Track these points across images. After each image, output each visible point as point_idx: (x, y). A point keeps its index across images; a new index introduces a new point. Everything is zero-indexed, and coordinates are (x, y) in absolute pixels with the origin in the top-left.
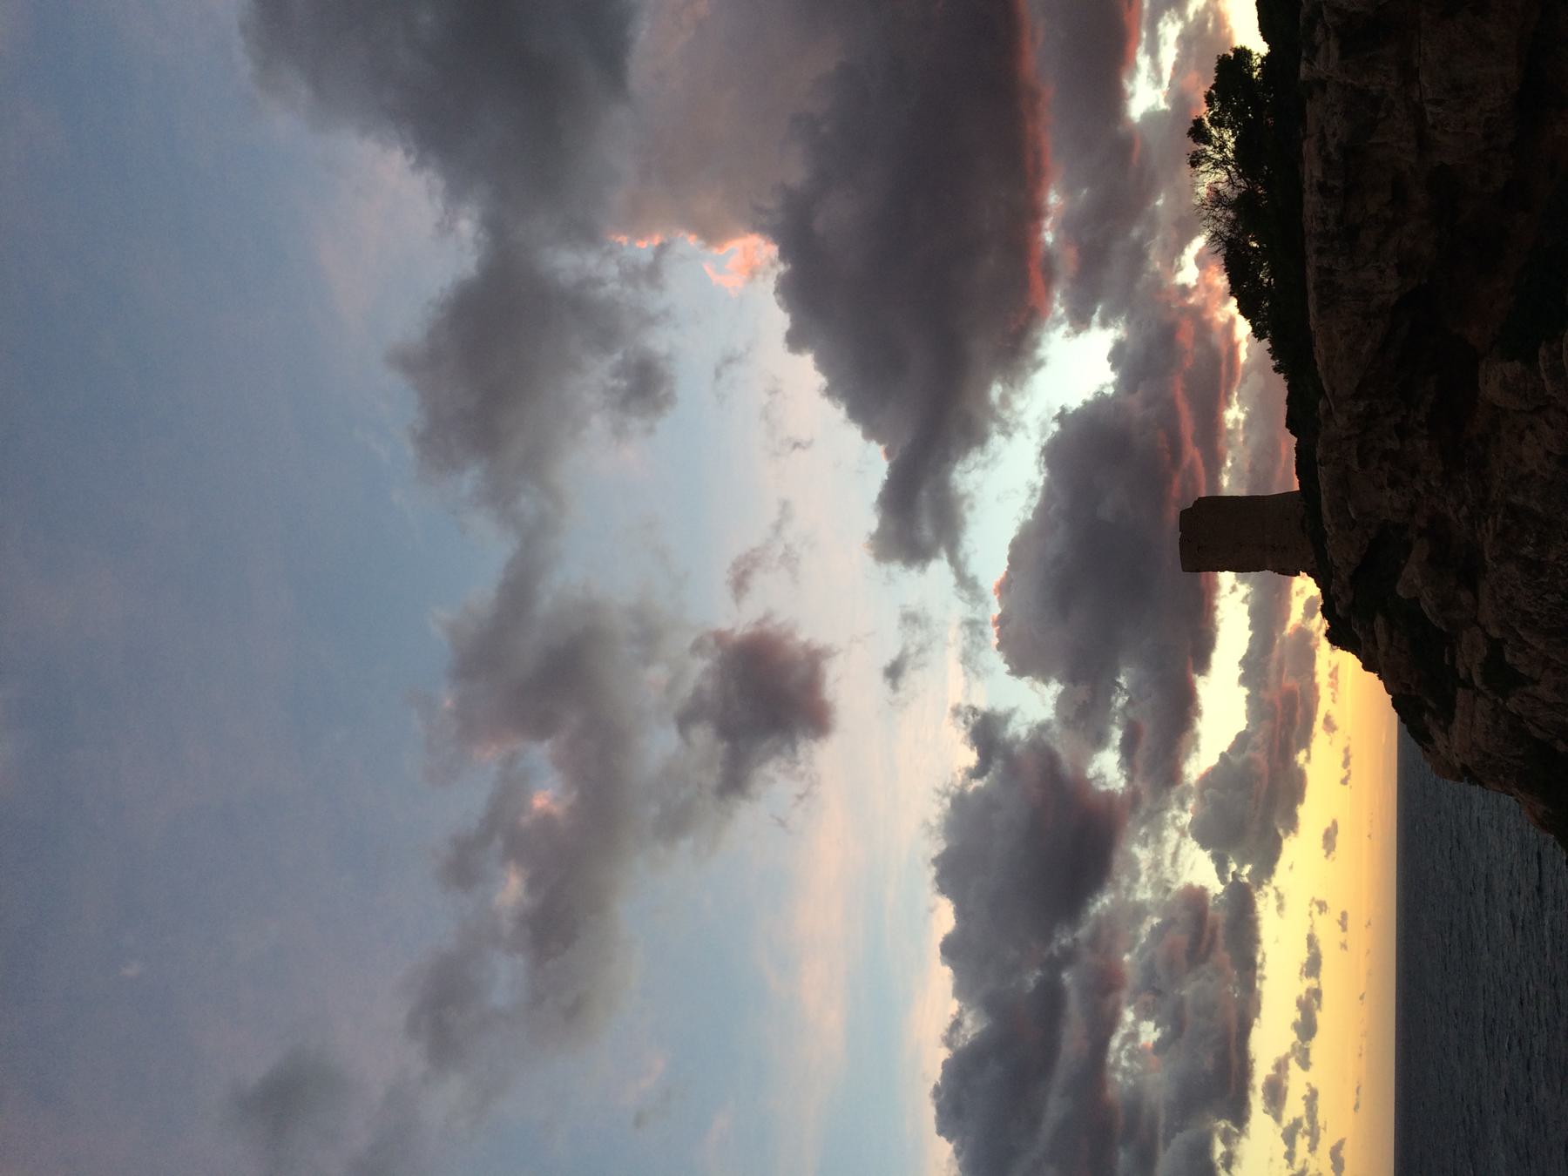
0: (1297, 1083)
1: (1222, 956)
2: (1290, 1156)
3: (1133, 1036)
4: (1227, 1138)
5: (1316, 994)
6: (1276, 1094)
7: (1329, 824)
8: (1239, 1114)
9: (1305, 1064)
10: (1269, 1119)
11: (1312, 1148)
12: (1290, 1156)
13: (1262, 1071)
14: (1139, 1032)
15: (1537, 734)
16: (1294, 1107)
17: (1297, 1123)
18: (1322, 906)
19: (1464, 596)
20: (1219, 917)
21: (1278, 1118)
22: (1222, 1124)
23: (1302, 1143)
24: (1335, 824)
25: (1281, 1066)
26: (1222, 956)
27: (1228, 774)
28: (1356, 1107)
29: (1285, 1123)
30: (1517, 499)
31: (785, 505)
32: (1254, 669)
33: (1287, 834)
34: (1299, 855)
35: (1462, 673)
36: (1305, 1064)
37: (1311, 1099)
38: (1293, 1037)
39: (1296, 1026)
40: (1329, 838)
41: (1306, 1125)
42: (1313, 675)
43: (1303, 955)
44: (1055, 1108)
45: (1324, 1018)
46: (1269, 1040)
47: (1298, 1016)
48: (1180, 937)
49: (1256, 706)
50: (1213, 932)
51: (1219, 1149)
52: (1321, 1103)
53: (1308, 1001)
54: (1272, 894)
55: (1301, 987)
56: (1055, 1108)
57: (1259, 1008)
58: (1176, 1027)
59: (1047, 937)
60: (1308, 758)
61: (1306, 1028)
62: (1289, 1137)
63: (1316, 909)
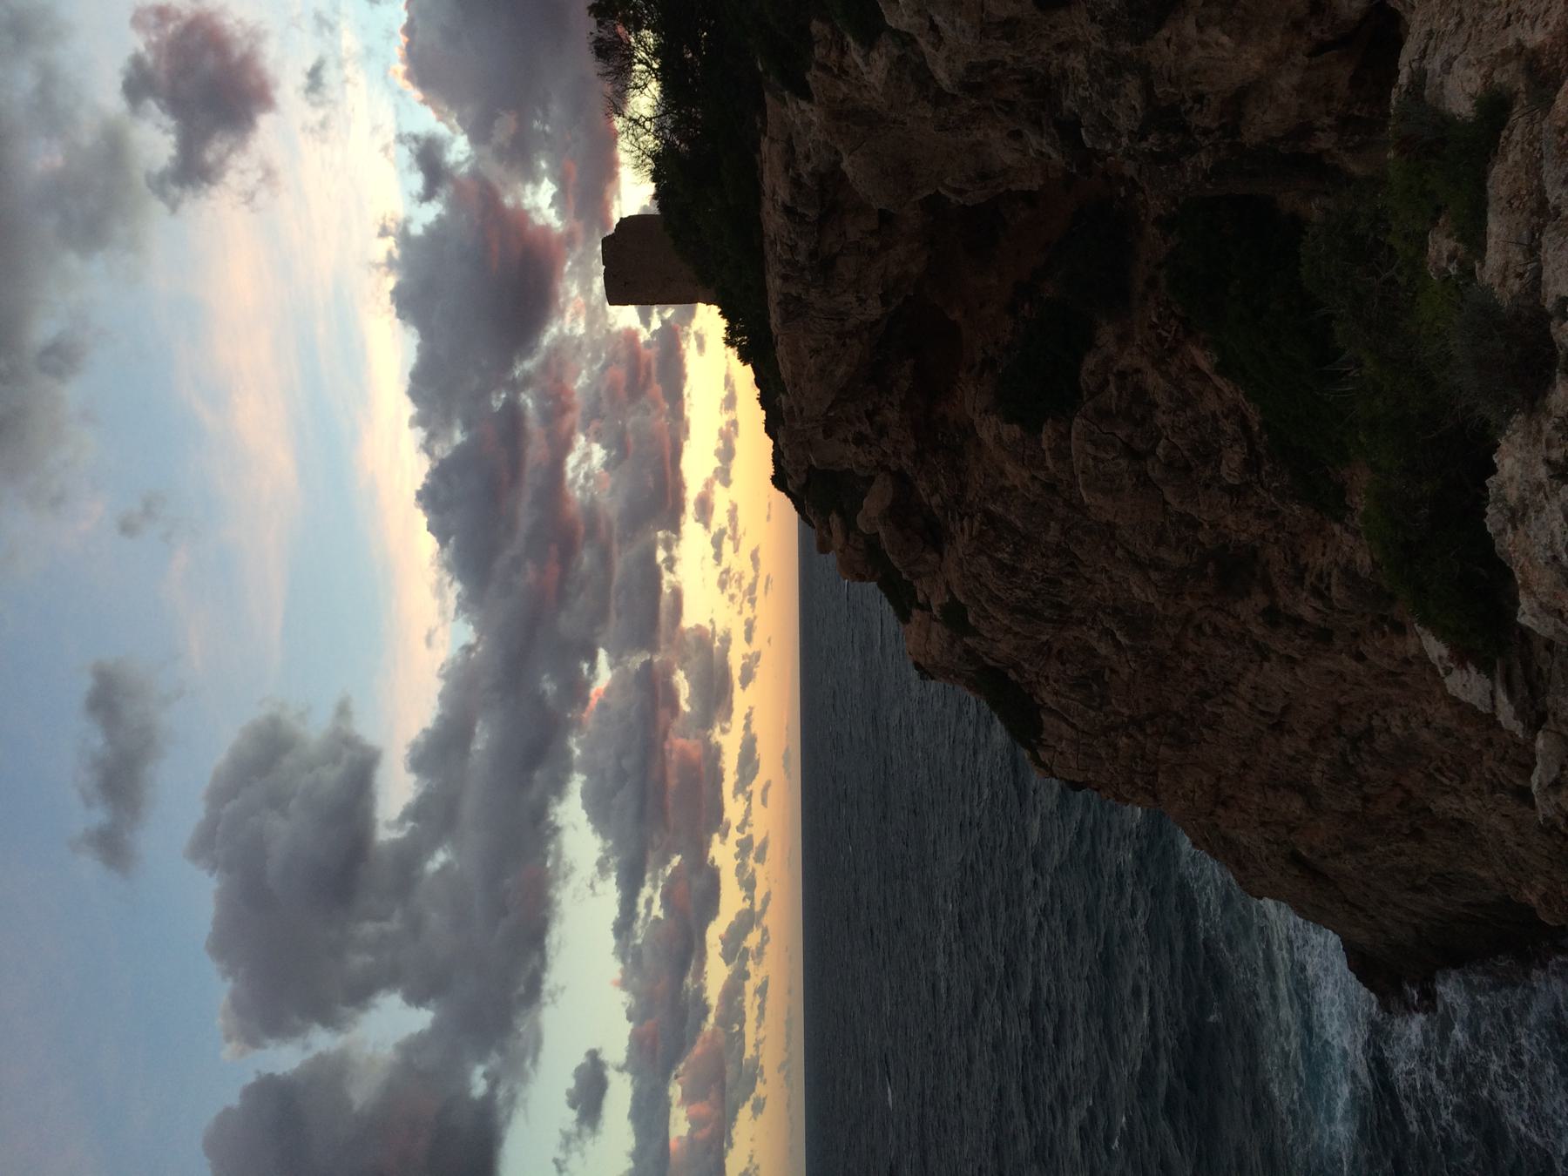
0: (721, 499)
1: (656, 388)
2: (718, 557)
3: (587, 456)
4: (668, 546)
5: (734, 424)
6: (705, 509)
8: (673, 524)
9: (727, 482)
10: (700, 526)
11: (736, 550)
12: (718, 557)
13: (692, 492)
14: (587, 460)
15: (990, 662)
16: (720, 518)
17: (722, 532)
19: (931, 557)
20: (652, 354)
21: (707, 526)
22: (660, 534)
23: (727, 546)
25: (708, 485)
26: (656, 388)
28: (768, 518)
29: (714, 528)
30: (997, 508)
31: (109, 698)
35: (921, 597)
36: (727, 482)
37: (733, 514)
38: (716, 463)
39: (718, 453)
41: (729, 531)
43: (724, 394)
44: (525, 515)
45: (739, 444)
46: (696, 464)
47: (721, 444)
48: (620, 373)
50: (648, 366)
51: (661, 555)
52: (741, 514)
54: (692, 337)
55: (721, 420)
56: (525, 515)
57: (687, 431)
58: (620, 449)
59: (508, 365)
61: (727, 454)
62: (717, 543)
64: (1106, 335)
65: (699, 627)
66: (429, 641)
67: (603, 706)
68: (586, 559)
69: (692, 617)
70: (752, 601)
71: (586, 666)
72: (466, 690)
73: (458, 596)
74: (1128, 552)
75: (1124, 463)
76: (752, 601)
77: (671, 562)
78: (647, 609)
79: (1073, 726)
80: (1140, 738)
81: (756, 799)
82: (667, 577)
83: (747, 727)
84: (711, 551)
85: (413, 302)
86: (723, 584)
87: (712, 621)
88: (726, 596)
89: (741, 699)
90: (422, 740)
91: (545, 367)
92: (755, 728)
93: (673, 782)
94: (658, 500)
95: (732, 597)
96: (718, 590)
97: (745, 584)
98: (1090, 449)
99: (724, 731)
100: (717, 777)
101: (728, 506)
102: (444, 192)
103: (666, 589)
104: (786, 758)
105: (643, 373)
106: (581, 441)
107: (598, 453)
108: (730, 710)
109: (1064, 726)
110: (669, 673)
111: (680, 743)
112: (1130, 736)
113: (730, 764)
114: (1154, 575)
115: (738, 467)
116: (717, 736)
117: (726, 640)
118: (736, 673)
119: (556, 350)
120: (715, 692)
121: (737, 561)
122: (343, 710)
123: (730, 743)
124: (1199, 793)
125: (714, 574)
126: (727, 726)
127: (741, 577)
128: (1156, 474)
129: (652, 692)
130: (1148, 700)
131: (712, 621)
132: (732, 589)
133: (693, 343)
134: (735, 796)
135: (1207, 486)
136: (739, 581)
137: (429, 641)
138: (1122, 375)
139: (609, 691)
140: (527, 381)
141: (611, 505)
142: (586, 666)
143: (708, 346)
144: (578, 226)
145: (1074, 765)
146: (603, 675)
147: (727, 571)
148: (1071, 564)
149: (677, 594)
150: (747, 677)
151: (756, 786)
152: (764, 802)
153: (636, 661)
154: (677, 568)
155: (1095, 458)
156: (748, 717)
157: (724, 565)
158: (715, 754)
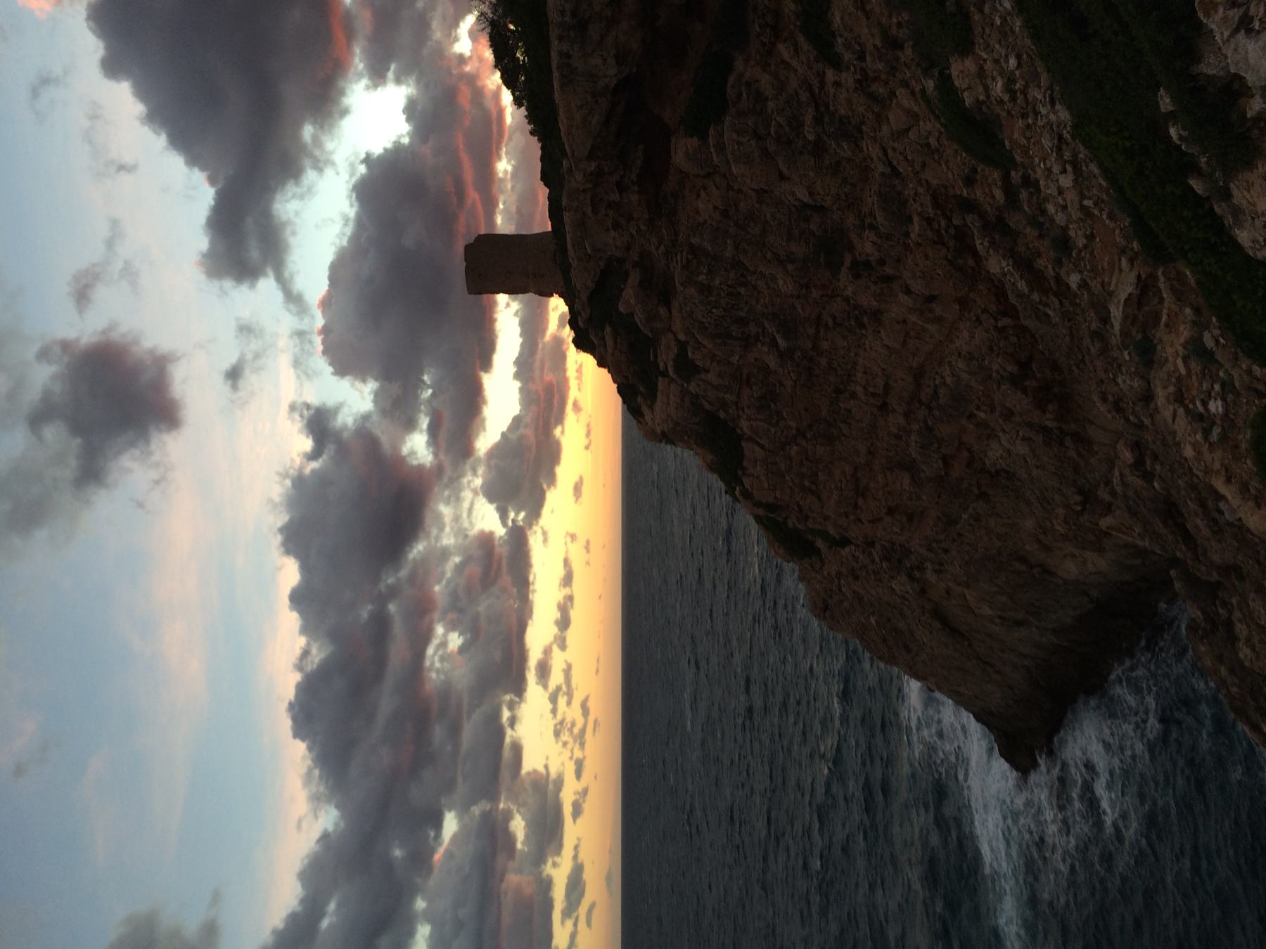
0: (558, 661)
1: (506, 579)
2: (554, 711)
3: (444, 644)
4: (511, 706)
5: (570, 598)
6: (544, 670)
7: (576, 478)
8: (519, 688)
9: (563, 647)
10: (540, 688)
11: (569, 703)
12: (554, 711)
14: (446, 642)
16: (556, 678)
17: (558, 689)
18: (573, 537)
19: (663, 311)
20: (502, 551)
21: (545, 687)
23: (562, 701)
24: (581, 479)
25: (547, 651)
26: (506, 579)
27: (508, 448)
28: (597, 671)
30: (695, 240)
32: (524, 367)
33: (549, 487)
34: (558, 500)
36: (563, 647)
37: (568, 671)
38: (555, 630)
39: (557, 623)
40: (578, 489)
41: (564, 688)
42: (565, 370)
44: (386, 703)
47: (558, 615)
48: (476, 569)
49: (527, 397)
51: (506, 714)
52: (574, 672)
53: (565, 604)
56: (386, 703)
60: (563, 432)
61: (564, 623)
62: (553, 699)
63: (569, 539)
64: (739, 65)
65: (535, 771)
66: (299, 826)
67: (449, 855)
68: (438, 732)
69: (532, 762)
70: (582, 745)
71: (432, 834)
72: (328, 868)
73: (325, 837)
74: (774, 254)
75: (753, 142)
76: (582, 745)
77: (513, 721)
78: (495, 759)
79: (762, 447)
80: (804, 443)
81: (582, 919)
82: (509, 732)
83: (575, 857)
84: (550, 706)
85: (296, 538)
86: (557, 734)
87: (546, 767)
88: (560, 744)
89: (572, 831)
90: (341, 84)
91: (412, 578)
92: (581, 856)
93: (507, 918)
94: (505, 668)
95: (565, 744)
96: (553, 739)
97: (576, 731)
98: (734, 136)
99: (555, 865)
100: (548, 905)
101: (564, 666)
102: (330, 449)
103: (508, 740)
104: (609, 878)
105: (495, 566)
106: (440, 630)
107: (455, 641)
108: (560, 846)
109: (757, 448)
110: (508, 816)
111: (515, 880)
112: (797, 445)
113: (559, 894)
114: (790, 267)
115: (572, 635)
116: (548, 869)
117: (559, 783)
118: (567, 810)
119: (423, 562)
120: (548, 829)
121: (573, 713)
122: (216, 898)
123: (559, 872)
124: (844, 482)
125: (550, 724)
126: (557, 859)
127: (573, 724)
128: (772, 148)
129: (490, 839)
130: (806, 410)
131: (546, 767)
132: (565, 737)
133: (539, 536)
134: (563, 923)
135: (801, 153)
136: (571, 730)
137: (299, 826)
138: (748, 84)
139: (455, 838)
140: (393, 593)
141: (462, 676)
142: (432, 834)
143: (550, 540)
144: (446, 460)
145: (766, 485)
146: (451, 825)
147: (562, 722)
148: (743, 275)
149: (517, 749)
150: (577, 811)
151: (583, 910)
152: (589, 923)
153: (476, 810)
154: (517, 726)
155: (738, 143)
156: (576, 848)
157: (559, 717)
158: (546, 885)
